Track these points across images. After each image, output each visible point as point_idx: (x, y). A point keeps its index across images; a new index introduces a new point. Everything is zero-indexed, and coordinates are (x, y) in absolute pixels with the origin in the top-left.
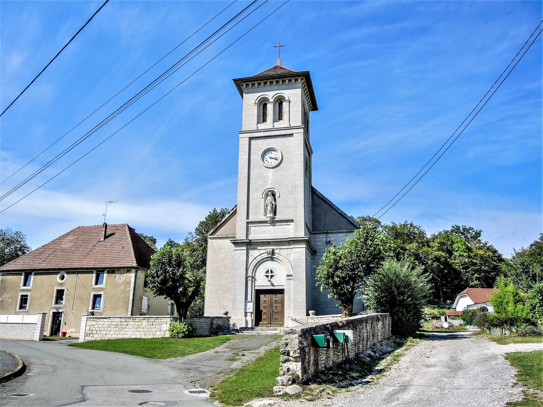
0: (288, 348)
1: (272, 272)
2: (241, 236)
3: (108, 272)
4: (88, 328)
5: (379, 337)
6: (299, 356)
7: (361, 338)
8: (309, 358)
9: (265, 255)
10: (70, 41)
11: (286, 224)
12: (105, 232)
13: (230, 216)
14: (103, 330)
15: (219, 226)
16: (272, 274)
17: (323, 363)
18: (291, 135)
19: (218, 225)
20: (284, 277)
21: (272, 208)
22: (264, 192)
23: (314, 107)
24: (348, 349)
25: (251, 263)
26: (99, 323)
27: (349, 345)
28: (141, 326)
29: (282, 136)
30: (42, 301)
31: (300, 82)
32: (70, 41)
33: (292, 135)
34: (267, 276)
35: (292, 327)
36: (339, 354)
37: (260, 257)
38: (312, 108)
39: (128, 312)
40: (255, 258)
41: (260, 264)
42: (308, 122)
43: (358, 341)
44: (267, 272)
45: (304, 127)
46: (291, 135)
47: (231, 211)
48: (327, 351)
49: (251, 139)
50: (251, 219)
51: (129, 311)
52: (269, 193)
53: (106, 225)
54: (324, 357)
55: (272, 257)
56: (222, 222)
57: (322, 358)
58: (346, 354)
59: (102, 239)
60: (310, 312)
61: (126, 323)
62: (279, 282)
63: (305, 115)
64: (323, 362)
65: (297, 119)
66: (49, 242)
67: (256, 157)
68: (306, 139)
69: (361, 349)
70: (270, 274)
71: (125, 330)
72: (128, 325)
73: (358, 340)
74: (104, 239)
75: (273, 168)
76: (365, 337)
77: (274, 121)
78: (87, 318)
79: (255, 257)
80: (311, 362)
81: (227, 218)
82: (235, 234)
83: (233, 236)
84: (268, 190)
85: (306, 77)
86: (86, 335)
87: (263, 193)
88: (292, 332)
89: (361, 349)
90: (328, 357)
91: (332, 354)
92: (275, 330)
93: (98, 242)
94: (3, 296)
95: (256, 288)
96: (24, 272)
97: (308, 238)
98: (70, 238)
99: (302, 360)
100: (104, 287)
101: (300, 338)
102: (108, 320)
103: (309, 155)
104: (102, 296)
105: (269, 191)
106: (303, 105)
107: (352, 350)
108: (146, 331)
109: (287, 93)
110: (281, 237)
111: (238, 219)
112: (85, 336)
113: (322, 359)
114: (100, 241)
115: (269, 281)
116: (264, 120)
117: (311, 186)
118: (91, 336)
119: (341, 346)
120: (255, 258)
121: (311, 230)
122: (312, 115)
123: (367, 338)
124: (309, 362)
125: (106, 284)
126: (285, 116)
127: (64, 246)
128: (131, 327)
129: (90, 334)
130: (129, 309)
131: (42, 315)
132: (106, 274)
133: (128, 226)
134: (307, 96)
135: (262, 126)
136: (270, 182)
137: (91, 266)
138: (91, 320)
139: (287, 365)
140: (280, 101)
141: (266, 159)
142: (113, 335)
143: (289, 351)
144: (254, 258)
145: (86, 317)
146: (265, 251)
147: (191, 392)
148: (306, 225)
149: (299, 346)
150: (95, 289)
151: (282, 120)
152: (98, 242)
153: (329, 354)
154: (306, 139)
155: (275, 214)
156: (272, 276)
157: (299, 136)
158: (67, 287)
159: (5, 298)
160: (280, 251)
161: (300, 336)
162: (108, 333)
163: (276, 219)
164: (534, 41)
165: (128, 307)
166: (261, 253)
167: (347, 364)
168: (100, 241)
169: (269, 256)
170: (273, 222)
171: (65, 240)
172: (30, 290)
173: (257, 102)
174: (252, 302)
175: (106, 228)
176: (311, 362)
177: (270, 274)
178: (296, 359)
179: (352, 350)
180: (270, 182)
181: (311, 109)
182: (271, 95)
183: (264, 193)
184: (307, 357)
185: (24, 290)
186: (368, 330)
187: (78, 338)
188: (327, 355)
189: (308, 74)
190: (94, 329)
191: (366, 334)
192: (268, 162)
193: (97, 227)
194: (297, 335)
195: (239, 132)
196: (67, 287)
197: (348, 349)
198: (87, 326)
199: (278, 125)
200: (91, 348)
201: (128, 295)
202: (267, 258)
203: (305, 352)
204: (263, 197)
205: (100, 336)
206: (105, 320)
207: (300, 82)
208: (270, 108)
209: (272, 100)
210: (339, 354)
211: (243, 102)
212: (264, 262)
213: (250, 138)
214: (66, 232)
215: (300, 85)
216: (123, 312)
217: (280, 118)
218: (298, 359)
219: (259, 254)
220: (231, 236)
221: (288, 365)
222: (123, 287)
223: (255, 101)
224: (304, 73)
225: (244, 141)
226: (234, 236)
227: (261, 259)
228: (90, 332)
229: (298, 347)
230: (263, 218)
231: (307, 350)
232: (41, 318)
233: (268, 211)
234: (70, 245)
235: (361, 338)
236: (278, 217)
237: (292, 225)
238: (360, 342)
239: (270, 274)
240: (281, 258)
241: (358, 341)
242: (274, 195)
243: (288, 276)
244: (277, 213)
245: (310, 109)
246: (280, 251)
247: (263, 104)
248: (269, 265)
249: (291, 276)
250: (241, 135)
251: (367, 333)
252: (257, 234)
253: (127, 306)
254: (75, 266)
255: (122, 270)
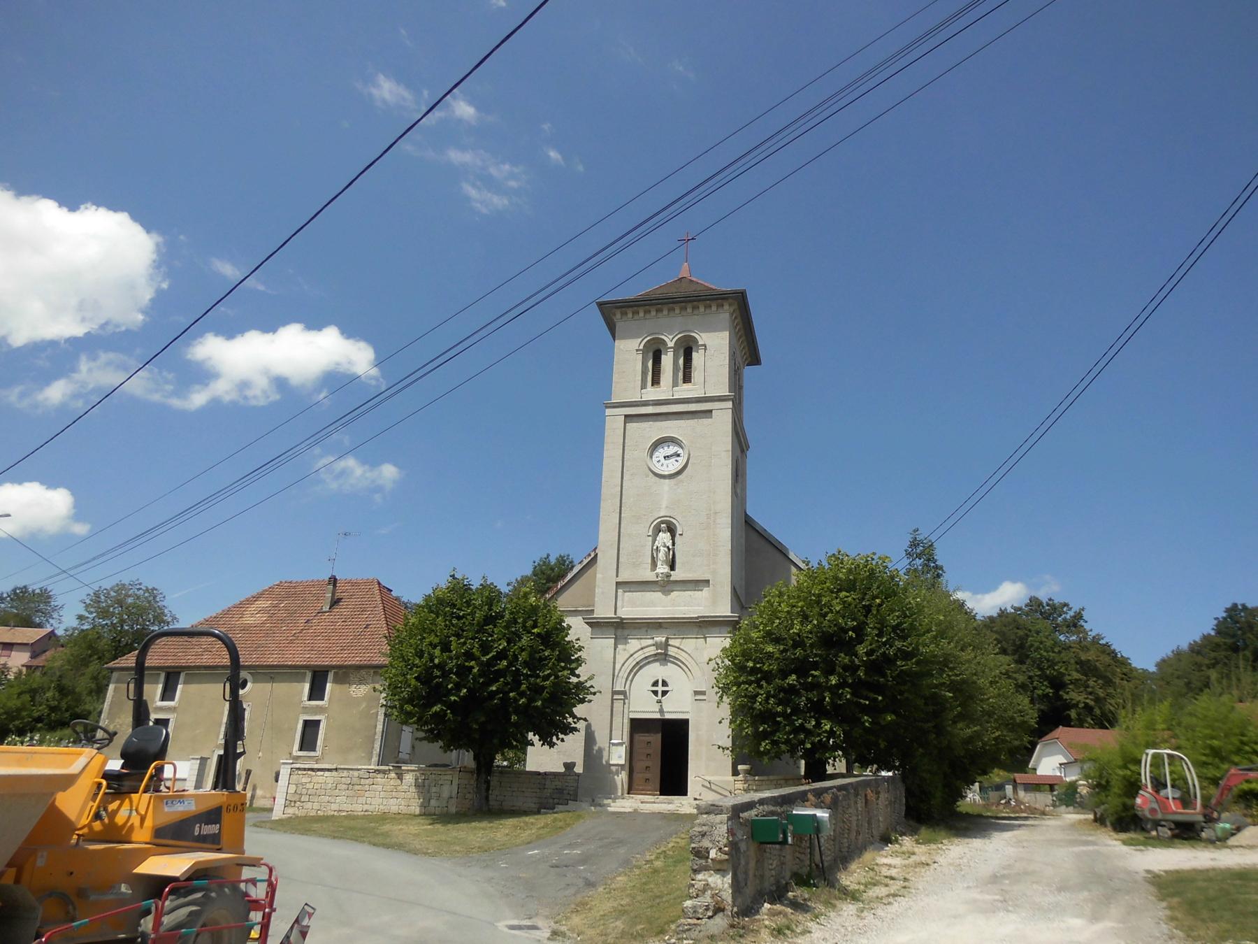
0: (706, 843)
1: (665, 684)
2: (603, 611)
4: (292, 789)
5: (881, 824)
6: (727, 860)
7: (846, 827)
8: (747, 863)
9: (652, 651)
10: (503, 42)
12: (333, 594)
13: (583, 568)
14: (324, 793)
15: (562, 587)
16: (665, 689)
17: (772, 876)
18: (708, 413)
19: (559, 587)
20: (689, 696)
21: (667, 554)
22: (652, 523)
23: (754, 359)
24: (820, 847)
25: (620, 670)
26: (315, 779)
27: (822, 840)
28: (400, 787)
29: (690, 416)
30: (198, 731)
31: (725, 315)
32: (503, 42)
33: (708, 414)
34: (655, 693)
35: (714, 801)
36: (802, 857)
37: (640, 652)
38: (749, 359)
39: (372, 758)
40: (632, 655)
41: (641, 668)
42: (741, 388)
43: (840, 833)
44: (655, 684)
45: (732, 397)
46: (708, 413)
47: (585, 558)
48: (781, 850)
49: (628, 418)
50: (625, 576)
51: (374, 756)
52: (662, 525)
53: (333, 581)
54: (775, 862)
55: (663, 657)
56: (566, 580)
57: (771, 864)
58: (817, 858)
59: (326, 608)
60: (740, 767)
61: (370, 781)
62: (674, 708)
63: (735, 374)
64: (773, 873)
65: (720, 386)
66: (219, 611)
67: (637, 453)
68: (736, 419)
69: (846, 849)
70: (660, 689)
71: (367, 794)
72: (373, 784)
73: (841, 831)
74: (330, 608)
75: (671, 476)
76: (854, 824)
77: (675, 384)
78: (292, 769)
79: (632, 652)
80: (751, 873)
81: (578, 573)
82: (594, 606)
83: (587, 609)
84: (659, 520)
85: (739, 304)
86: (289, 803)
88: (713, 809)
89: (846, 849)
90: (783, 863)
91: (789, 857)
92: (669, 803)
93: (318, 613)
94: (117, 720)
95: (633, 716)
96: (163, 671)
97: (737, 619)
98: (263, 604)
99: (733, 866)
101: (730, 823)
102: (334, 773)
103: (743, 451)
104: (322, 725)
105: (662, 522)
106: (733, 356)
107: (830, 850)
108: (409, 797)
110: (684, 614)
111: (599, 576)
112: (285, 807)
113: (770, 867)
114: (321, 612)
115: (659, 702)
116: (656, 381)
117: (745, 512)
118: (296, 805)
119: (808, 842)
120: (632, 655)
121: (743, 600)
122: (749, 371)
123: (857, 826)
124: (746, 873)
125: (330, 699)
126: (697, 374)
127: (249, 620)
128: (380, 789)
129: (295, 802)
130: (374, 752)
131: (198, 761)
133: (379, 584)
134: (740, 337)
135: (651, 393)
136: (664, 504)
137: (298, 660)
138: (300, 772)
139: (703, 878)
140: (687, 349)
141: (658, 459)
142: (341, 804)
143: (707, 848)
144: (629, 655)
145: (290, 766)
146: (650, 642)
147: (512, 927)
148: (734, 591)
149: (728, 839)
151: (691, 382)
152: (318, 613)
153: (784, 857)
154: (736, 419)
155: (672, 567)
156: (664, 693)
157: (723, 417)
158: (250, 703)
159: (120, 725)
160: (681, 643)
161: (729, 819)
162: (333, 801)
163: (671, 579)
164: (1234, 215)
165: (373, 747)
166: (643, 646)
168: (321, 612)
169: (659, 651)
170: (666, 585)
171: (252, 608)
172: (175, 708)
173: (641, 347)
174: (624, 746)
175: (335, 586)
176: (751, 873)
177: (660, 688)
178: (719, 869)
179: (830, 850)
180: (664, 504)
181: (746, 363)
183: (653, 526)
184: (743, 862)
185: (161, 709)
186: (860, 809)
187: (271, 810)
188: (780, 860)
189: (743, 296)
190: (304, 791)
191: (855, 818)
192: (660, 463)
193: (319, 584)
194: (724, 817)
196: (250, 703)
197: (820, 847)
198: (290, 785)
199: (685, 391)
200: (305, 832)
202: (655, 655)
203: (740, 852)
204: (650, 534)
205: (316, 806)
206: (327, 774)
207: (725, 315)
208: (667, 360)
209: (671, 344)
210: (802, 857)
211: (614, 345)
212: (649, 663)
213: (626, 416)
214: (255, 593)
215: (727, 315)
217: (687, 378)
218: (725, 866)
219: (640, 647)
220: (584, 609)
221: (706, 877)
223: (638, 345)
224: (735, 292)
225: (614, 418)
226: (590, 609)
227: (643, 656)
228: (296, 798)
229: (725, 841)
230: (650, 576)
231: (743, 846)
232: (197, 767)
233: (659, 563)
234: (260, 618)
235: (846, 827)
236: (677, 575)
237: (705, 593)
238: (843, 834)
239: (660, 688)
240: (682, 656)
241: (840, 833)
242: (671, 530)
243: (696, 693)
244: (678, 565)
245: (744, 362)
246: (681, 643)
247: (655, 353)
248: (656, 671)
249: (703, 693)
250: (608, 412)
251: (858, 816)
252: (636, 607)
254: (273, 660)
255: (363, 672)
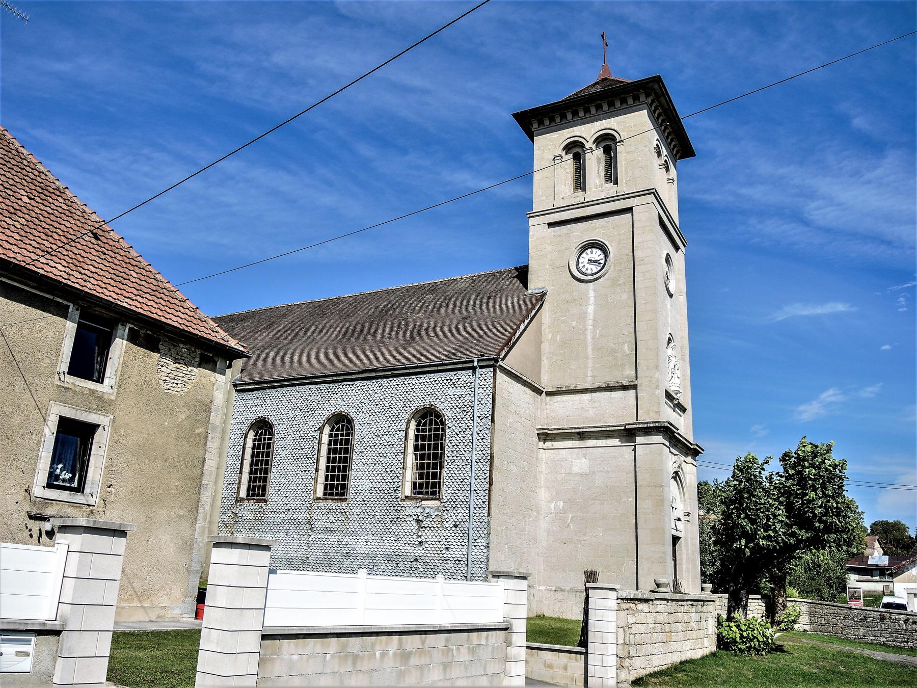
3: (133, 338)
11: (672, 427)
22: (584, 139)
39: (196, 520)
87: (582, 137)
100: (113, 398)
109: (619, 124)
132: (125, 342)
134: (656, 109)
140: (607, 142)
150: (70, 394)
165: (198, 501)
167: (890, 564)
182: (588, 131)
195: (528, 216)
201: (199, 454)
216: (180, 517)
222: (183, 416)
253: (193, 496)
